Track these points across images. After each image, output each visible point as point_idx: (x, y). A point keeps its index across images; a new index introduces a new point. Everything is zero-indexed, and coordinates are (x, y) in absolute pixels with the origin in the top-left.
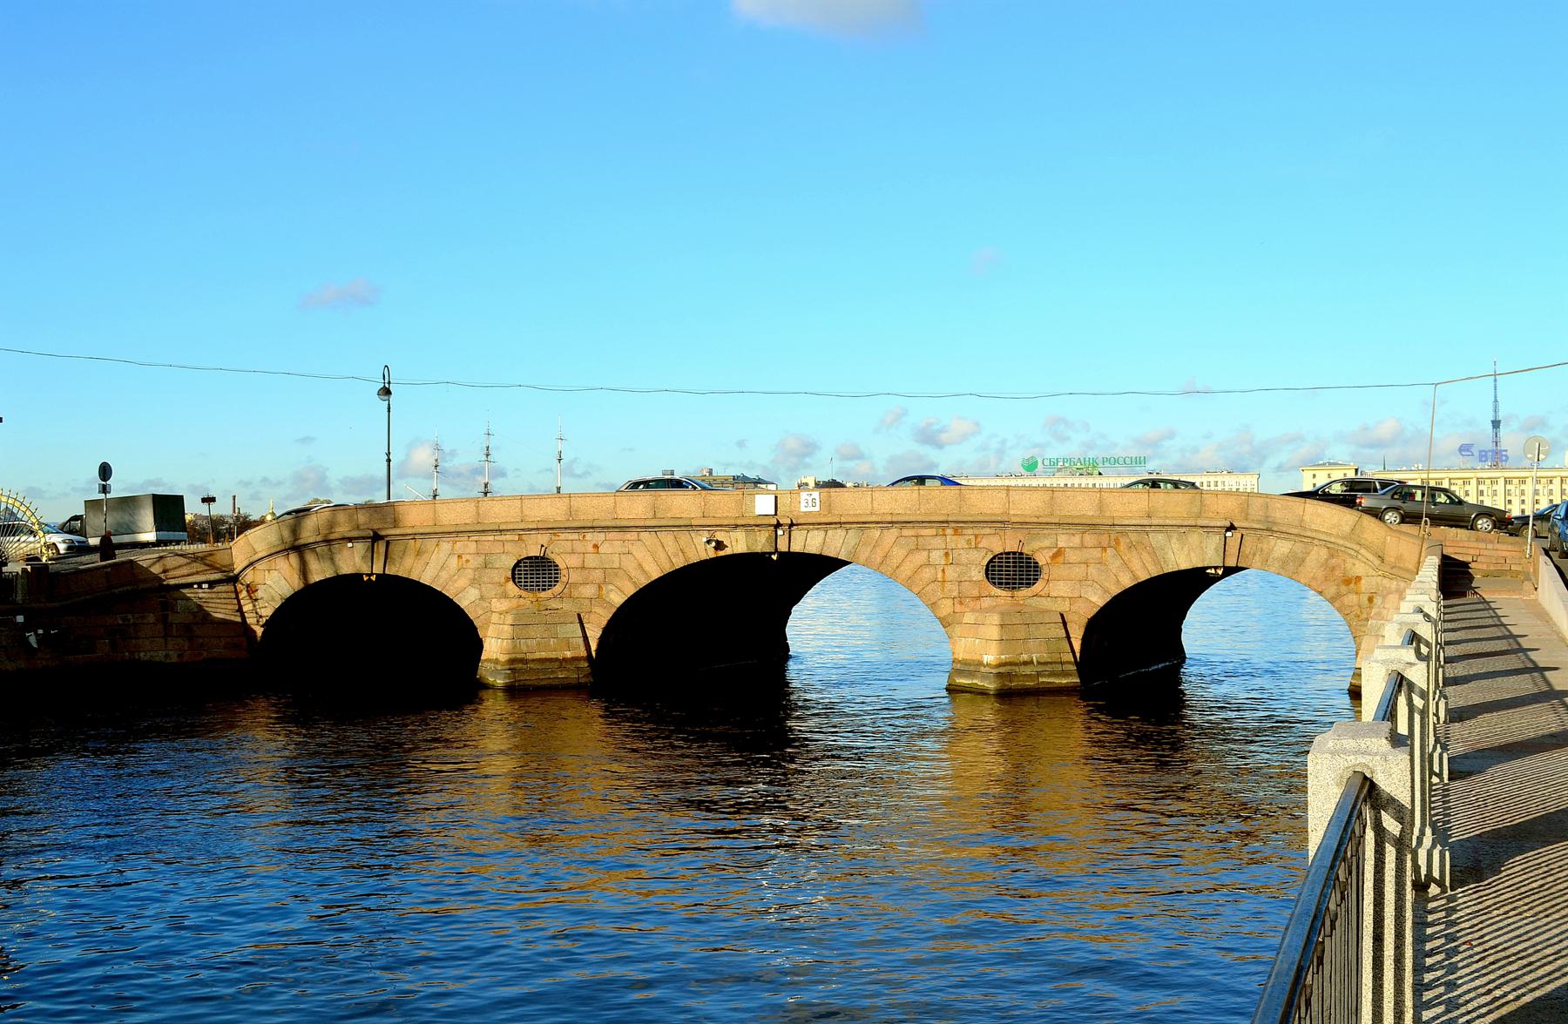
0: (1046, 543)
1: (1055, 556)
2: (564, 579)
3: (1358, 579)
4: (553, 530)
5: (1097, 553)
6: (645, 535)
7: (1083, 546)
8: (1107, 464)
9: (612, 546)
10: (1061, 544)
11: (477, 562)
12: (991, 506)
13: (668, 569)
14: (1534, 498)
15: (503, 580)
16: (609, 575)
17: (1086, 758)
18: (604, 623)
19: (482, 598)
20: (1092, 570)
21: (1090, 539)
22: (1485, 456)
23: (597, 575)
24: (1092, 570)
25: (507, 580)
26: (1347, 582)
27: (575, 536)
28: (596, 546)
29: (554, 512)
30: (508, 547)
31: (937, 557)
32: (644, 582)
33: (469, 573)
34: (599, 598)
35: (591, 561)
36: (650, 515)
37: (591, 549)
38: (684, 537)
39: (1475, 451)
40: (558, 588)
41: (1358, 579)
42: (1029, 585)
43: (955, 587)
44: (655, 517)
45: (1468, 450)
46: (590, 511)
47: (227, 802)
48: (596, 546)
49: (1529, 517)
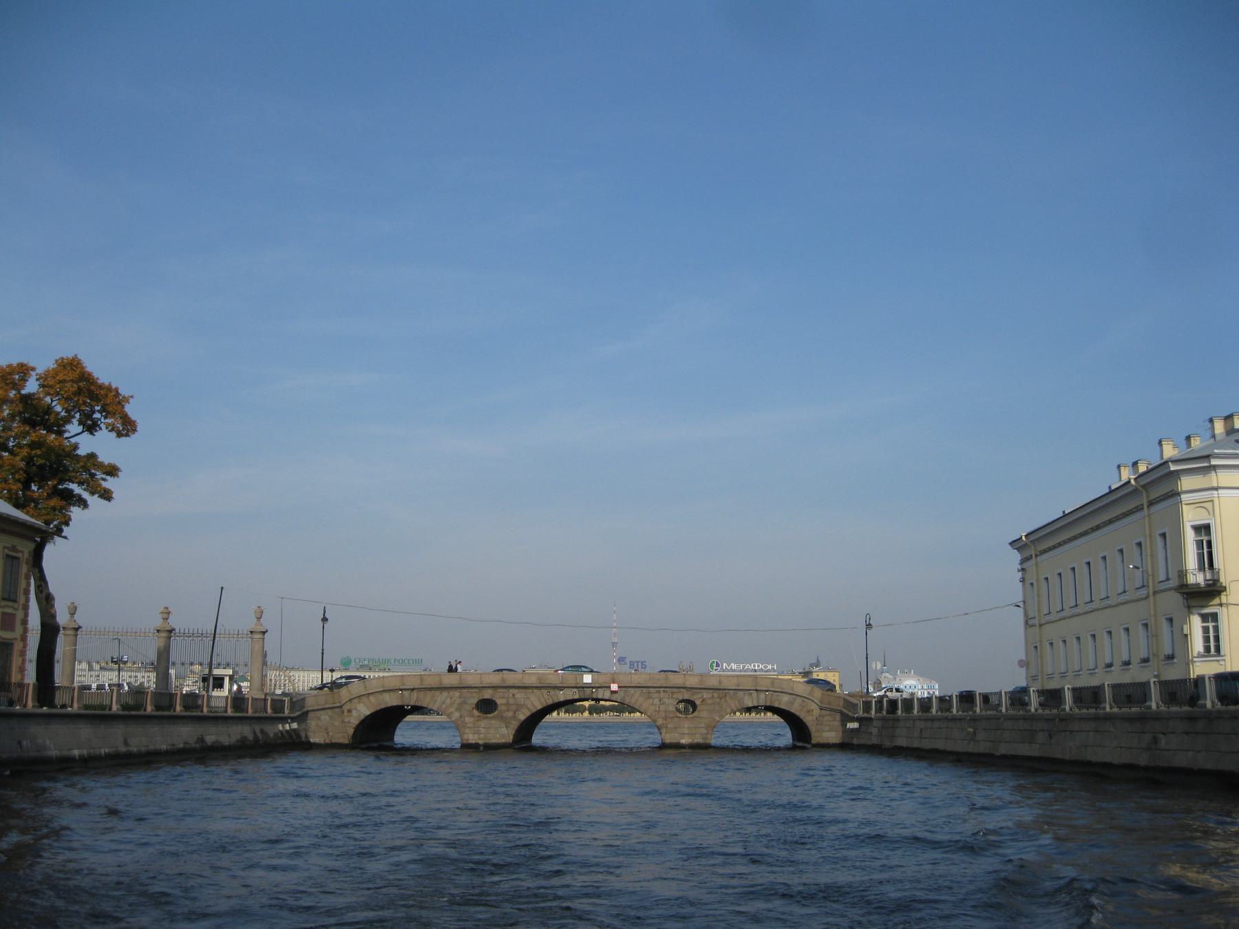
0: (699, 696)
1: (703, 701)
2: (499, 709)
3: (812, 710)
4: (495, 688)
5: (718, 700)
6: (535, 691)
7: (713, 697)
8: (397, 663)
9: (520, 695)
10: (704, 697)
11: (458, 701)
12: (471, 681)
13: (545, 705)
14: (226, 675)
15: (471, 709)
16: (519, 707)
17: (372, 855)
18: (516, 727)
19: (461, 716)
20: (717, 707)
21: (716, 695)
22: (633, 665)
23: (513, 707)
24: (717, 707)
25: (473, 709)
26: (809, 712)
27: (505, 690)
28: (513, 695)
29: (496, 679)
30: (474, 695)
31: (656, 701)
32: (534, 710)
33: (455, 706)
34: (514, 717)
35: (511, 701)
36: (538, 682)
37: (511, 696)
38: (552, 692)
39: (627, 661)
40: (496, 713)
41: (812, 710)
42: (492, 712)
43: (664, 714)
44: (540, 683)
45: (623, 661)
46: (430, 682)
47: (886, 820)
48: (513, 695)
49: (29, 684)
